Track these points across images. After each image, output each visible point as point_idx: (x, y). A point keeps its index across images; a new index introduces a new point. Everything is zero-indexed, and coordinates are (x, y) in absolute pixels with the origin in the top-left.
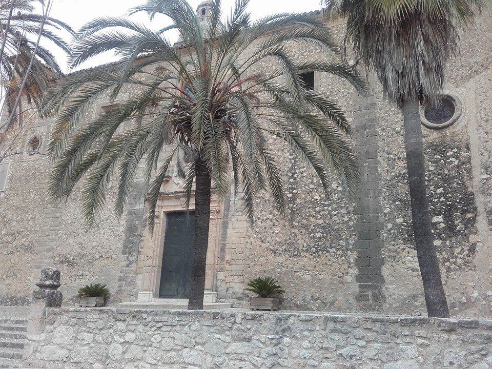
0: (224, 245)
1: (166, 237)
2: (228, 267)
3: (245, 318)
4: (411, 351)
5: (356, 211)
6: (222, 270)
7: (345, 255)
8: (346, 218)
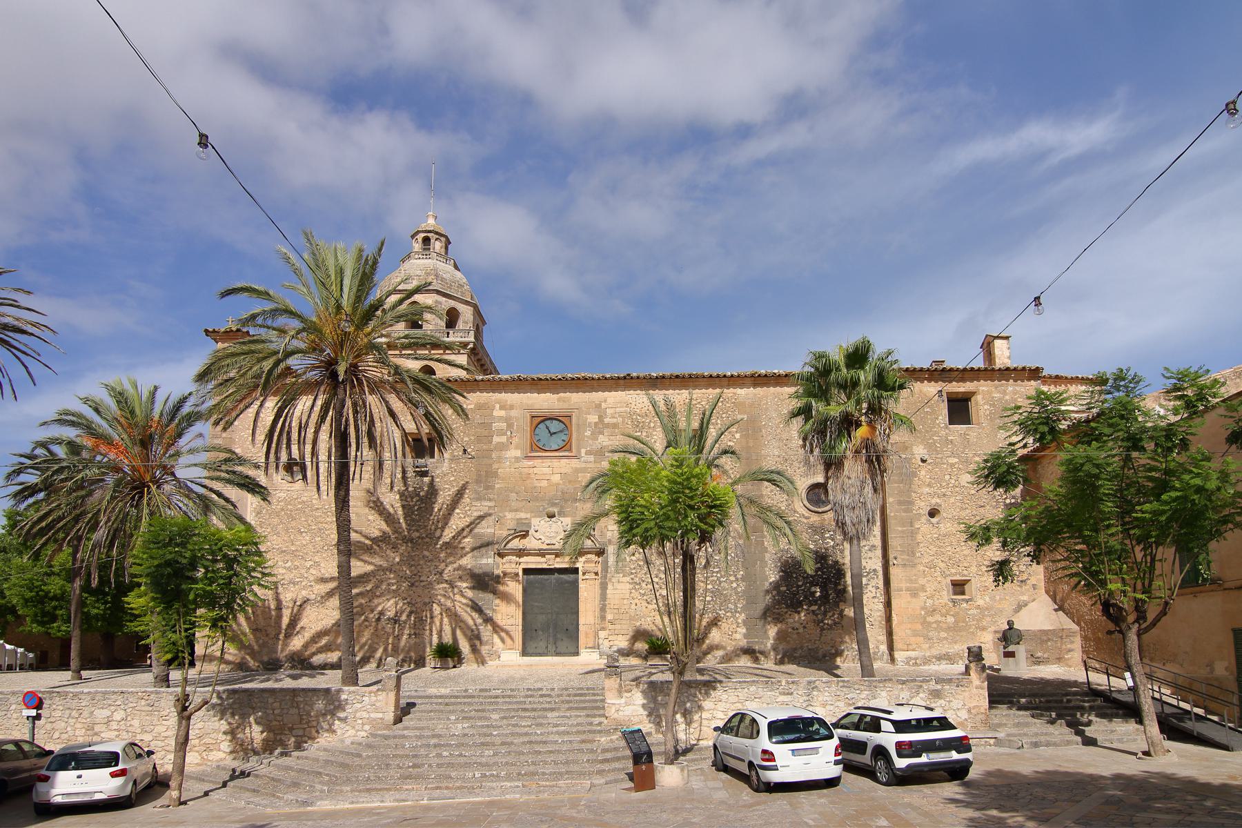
0: (604, 605)
1: (1236, 644)
2: (611, 627)
3: (788, 682)
4: (884, 694)
5: (743, 579)
6: (603, 629)
7: (734, 616)
8: (734, 585)
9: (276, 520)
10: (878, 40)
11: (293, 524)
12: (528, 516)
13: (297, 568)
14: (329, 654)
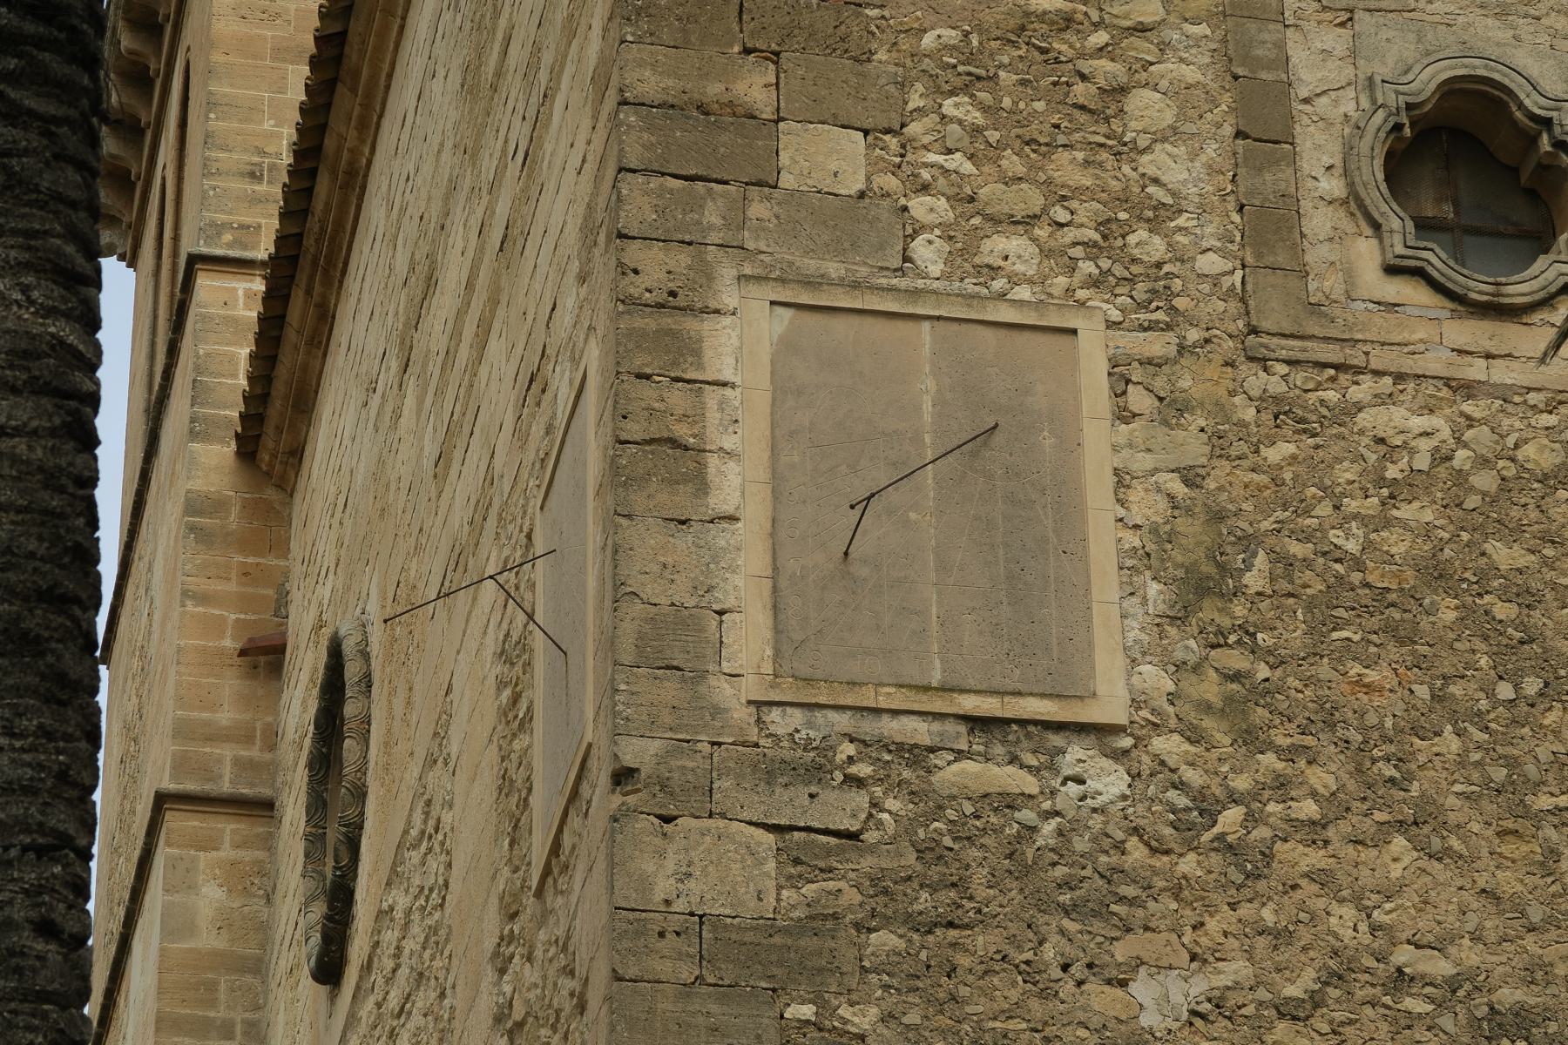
9: (1382, 686)
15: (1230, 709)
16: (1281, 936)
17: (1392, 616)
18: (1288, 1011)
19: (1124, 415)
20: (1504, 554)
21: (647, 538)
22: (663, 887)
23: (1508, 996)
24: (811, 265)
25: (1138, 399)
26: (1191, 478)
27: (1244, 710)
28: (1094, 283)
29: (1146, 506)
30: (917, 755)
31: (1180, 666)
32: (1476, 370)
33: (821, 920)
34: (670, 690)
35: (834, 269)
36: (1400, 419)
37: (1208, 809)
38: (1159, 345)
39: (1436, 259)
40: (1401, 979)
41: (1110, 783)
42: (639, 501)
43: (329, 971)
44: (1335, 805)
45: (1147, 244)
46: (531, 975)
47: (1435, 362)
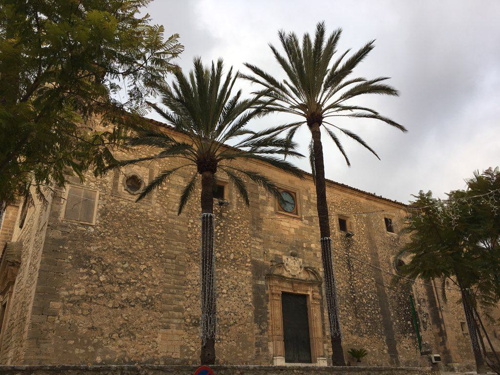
9: (117, 224)
10: (453, 192)
11: (132, 229)
12: (281, 254)
13: (132, 269)
14: (277, 148)
15: (104, 225)
16: (105, 244)
17: (119, 219)
18: (104, 250)
19: (99, 199)
20: (130, 215)
21: (55, 205)
22: (51, 235)
23: (123, 251)
24: (74, 183)
25: (101, 198)
26: (104, 205)
27: (105, 225)
28: (99, 188)
29: (100, 207)
30: (76, 226)
31: (100, 221)
32: (130, 199)
33: (64, 239)
34: (54, 218)
35: (76, 184)
36: (123, 202)
37: (100, 233)
38: (104, 194)
39: (129, 189)
40: (114, 249)
41: (93, 230)
42: (54, 202)
43: (21, 227)
44: (111, 234)
45: (104, 185)
46: (38, 238)
47: (127, 198)
